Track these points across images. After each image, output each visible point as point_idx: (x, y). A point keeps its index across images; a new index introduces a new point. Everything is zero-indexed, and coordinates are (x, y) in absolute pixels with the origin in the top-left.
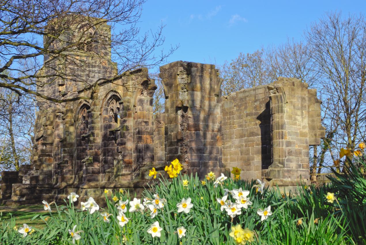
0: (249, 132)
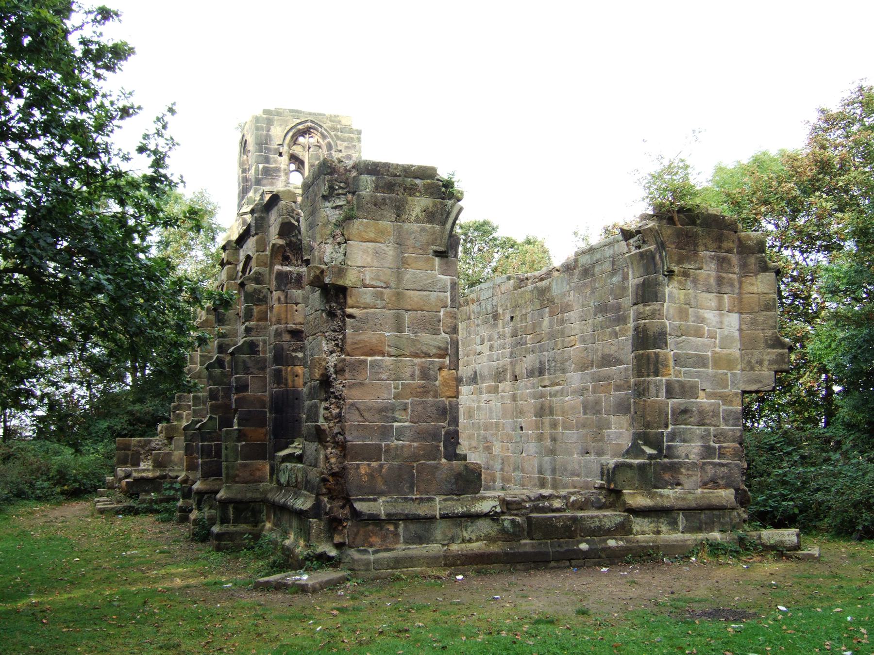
0: (599, 354)
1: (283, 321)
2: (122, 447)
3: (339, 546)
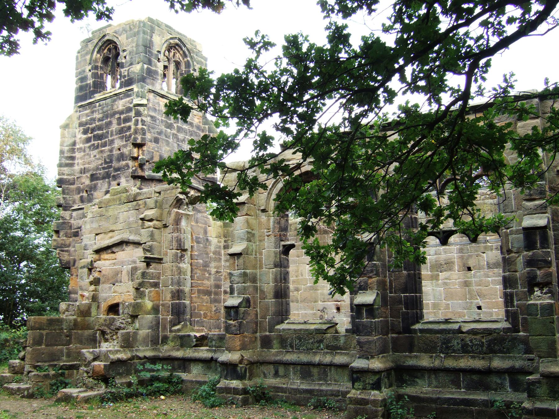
2: (37, 326)
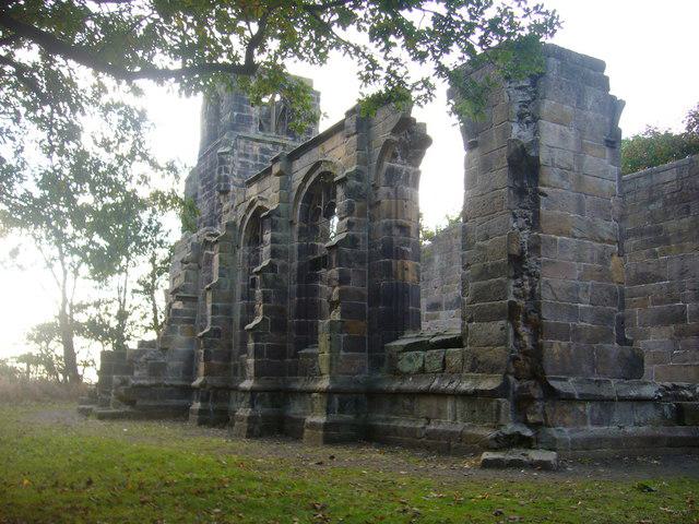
1: (394, 216)
3: (535, 426)
